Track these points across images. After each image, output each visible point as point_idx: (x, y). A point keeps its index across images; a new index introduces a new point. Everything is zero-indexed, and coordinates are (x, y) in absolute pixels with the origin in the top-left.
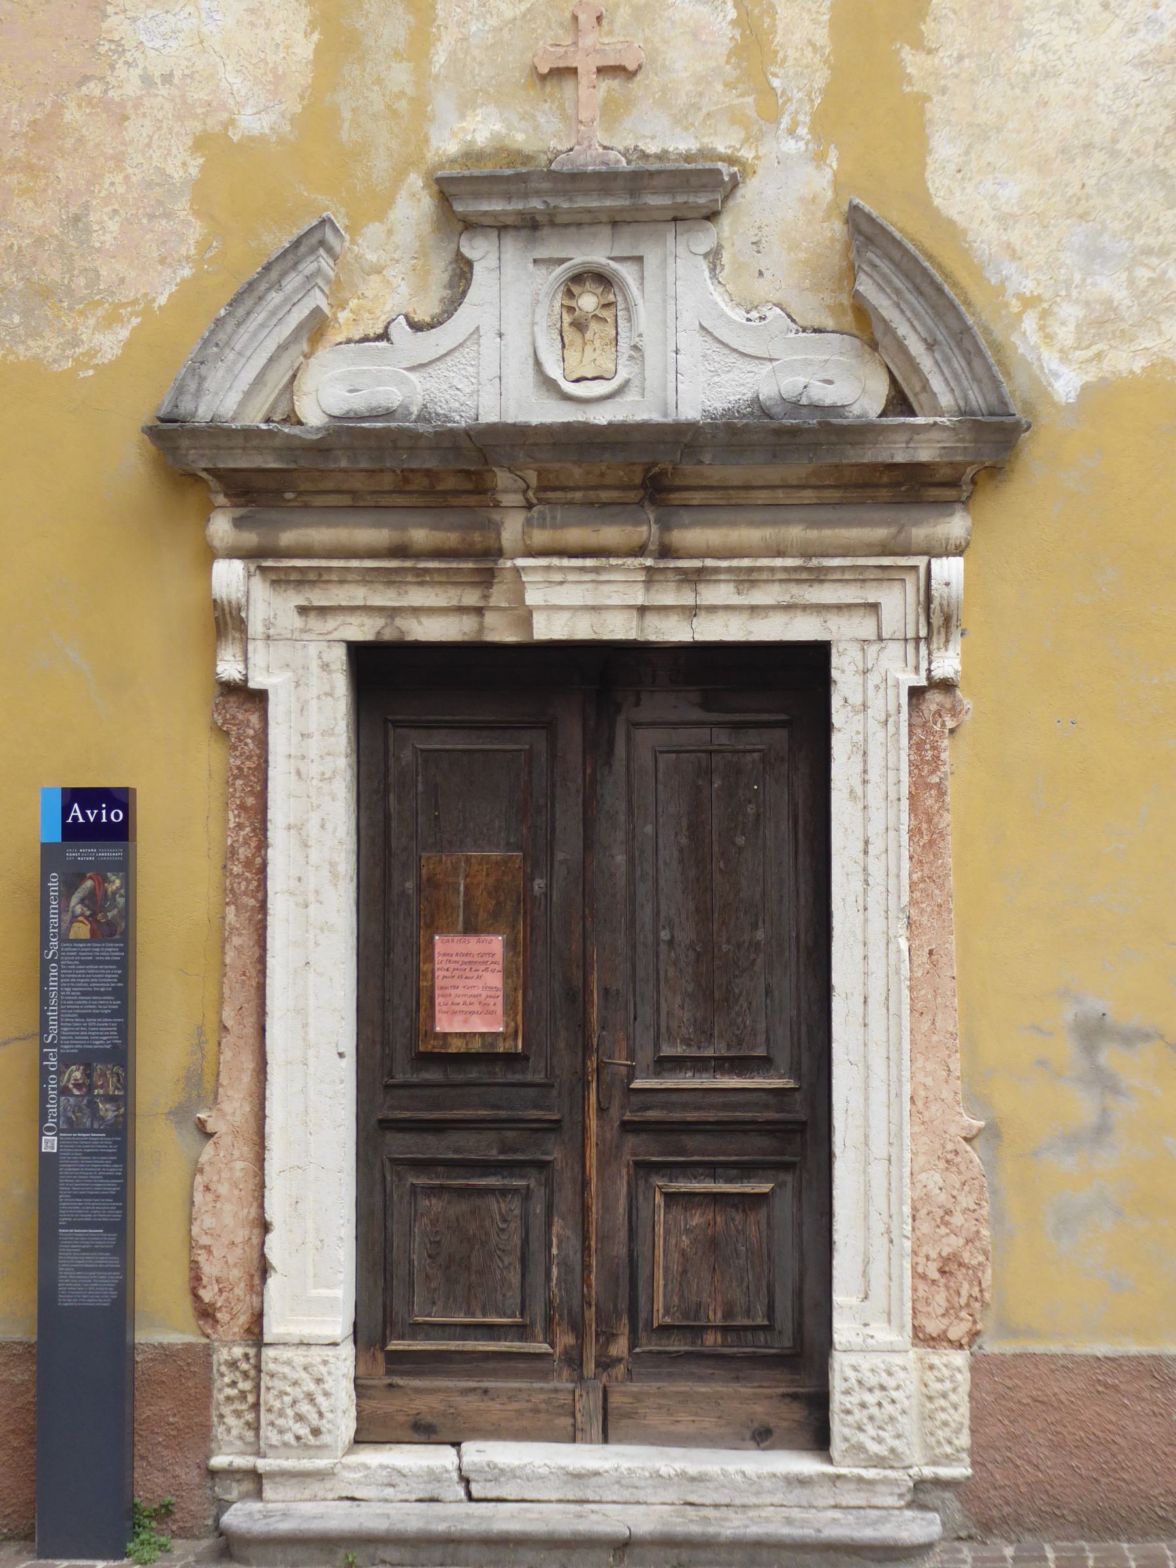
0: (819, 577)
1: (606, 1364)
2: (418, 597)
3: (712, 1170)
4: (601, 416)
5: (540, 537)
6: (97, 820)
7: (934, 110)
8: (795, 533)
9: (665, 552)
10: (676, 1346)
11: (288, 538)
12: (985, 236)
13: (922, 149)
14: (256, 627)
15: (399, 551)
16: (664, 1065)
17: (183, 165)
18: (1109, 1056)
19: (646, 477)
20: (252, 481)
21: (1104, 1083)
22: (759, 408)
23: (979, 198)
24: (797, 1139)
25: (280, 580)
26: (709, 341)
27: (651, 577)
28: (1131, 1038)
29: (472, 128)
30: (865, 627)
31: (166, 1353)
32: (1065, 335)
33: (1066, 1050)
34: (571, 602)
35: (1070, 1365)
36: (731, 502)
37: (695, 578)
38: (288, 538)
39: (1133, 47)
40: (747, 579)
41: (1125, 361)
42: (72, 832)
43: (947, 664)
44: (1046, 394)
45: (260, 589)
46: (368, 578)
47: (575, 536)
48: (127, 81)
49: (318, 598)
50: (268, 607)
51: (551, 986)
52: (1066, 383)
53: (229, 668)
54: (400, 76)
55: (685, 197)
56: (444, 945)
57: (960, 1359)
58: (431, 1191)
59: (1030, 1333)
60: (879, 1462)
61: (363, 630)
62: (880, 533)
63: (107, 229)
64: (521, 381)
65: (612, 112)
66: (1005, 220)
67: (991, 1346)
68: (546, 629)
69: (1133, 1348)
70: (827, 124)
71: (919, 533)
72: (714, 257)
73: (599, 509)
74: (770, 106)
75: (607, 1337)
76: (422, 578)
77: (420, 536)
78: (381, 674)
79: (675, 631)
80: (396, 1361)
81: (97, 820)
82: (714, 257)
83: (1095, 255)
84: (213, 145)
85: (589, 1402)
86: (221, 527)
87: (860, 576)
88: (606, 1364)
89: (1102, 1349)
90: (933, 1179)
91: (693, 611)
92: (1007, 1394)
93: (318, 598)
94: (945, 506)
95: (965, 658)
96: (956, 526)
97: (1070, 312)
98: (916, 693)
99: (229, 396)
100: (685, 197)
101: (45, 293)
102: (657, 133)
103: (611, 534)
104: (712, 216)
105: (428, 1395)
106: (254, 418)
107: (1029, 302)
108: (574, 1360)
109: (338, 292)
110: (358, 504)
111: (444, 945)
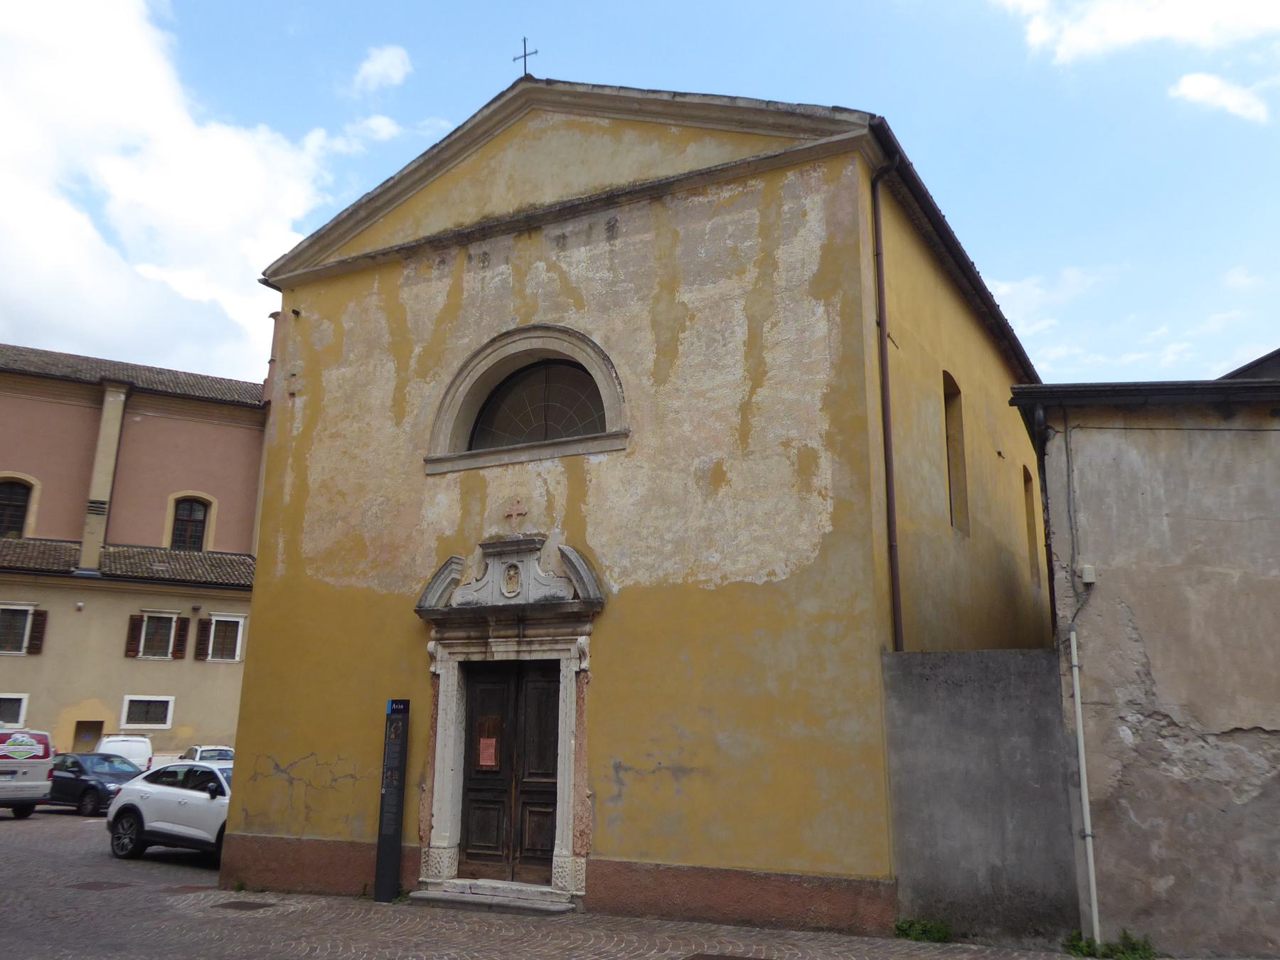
0: (557, 642)
1: (514, 859)
2: (472, 649)
3: (540, 805)
4: (513, 602)
5: (495, 634)
6: (400, 709)
7: (588, 520)
8: (552, 631)
9: (525, 636)
10: (530, 854)
11: (446, 635)
12: (598, 551)
13: (585, 530)
14: (439, 658)
15: (469, 638)
16: (531, 775)
17: (434, 544)
18: (622, 774)
19: (518, 618)
20: (445, 622)
21: (620, 782)
22: (546, 598)
23: (596, 540)
24: (549, 796)
25: (445, 646)
26: (537, 582)
27: (519, 643)
28: (627, 769)
29: (491, 531)
30: (567, 655)
31: (413, 849)
32: (616, 576)
33: (611, 772)
34: (502, 651)
35: (609, 863)
36: (539, 623)
37: (530, 643)
38: (446, 635)
39: (632, 500)
40: (541, 643)
41: (629, 582)
42: (394, 711)
43: (585, 665)
44: (610, 591)
45: (440, 648)
46: (462, 645)
47: (502, 633)
48: (425, 525)
49: (453, 650)
50: (441, 653)
51: (504, 754)
52: (615, 589)
53: (432, 669)
54: (478, 519)
55: (529, 546)
56: (483, 741)
57: (583, 860)
58: (479, 808)
59: (601, 854)
60: (562, 889)
61: (461, 658)
62: (570, 630)
63: (419, 561)
64: (496, 593)
65: (520, 525)
66: (602, 546)
67: (592, 858)
68: (497, 657)
69: (625, 860)
70: (565, 525)
71: (579, 630)
72: (538, 560)
73: (508, 626)
74: (553, 520)
75: (515, 851)
76: (473, 645)
77: (472, 634)
78: (468, 669)
79: (526, 657)
80: (469, 856)
81: (400, 709)
82: (538, 560)
83: (622, 555)
84: (441, 539)
85: (508, 870)
86: (433, 633)
87: (566, 642)
88: (514, 859)
89: (617, 859)
90: (579, 808)
91: (530, 652)
92: (596, 872)
93: (453, 650)
94: (586, 622)
95: (591, 664)
96: (587, 628)
97: (617, 570)
98: (577, 673)
99: (432, 601)
100: (529, 546)
101: (406, 576)
102: (530, 529)
103: (510, 632)
104: (539, 550)
105: (475, 865)
106: (440, 606)
107: (608, 567)
108: (507, 858)
109: (462, 572)
110: (461, 626)
111: (483, 741)
